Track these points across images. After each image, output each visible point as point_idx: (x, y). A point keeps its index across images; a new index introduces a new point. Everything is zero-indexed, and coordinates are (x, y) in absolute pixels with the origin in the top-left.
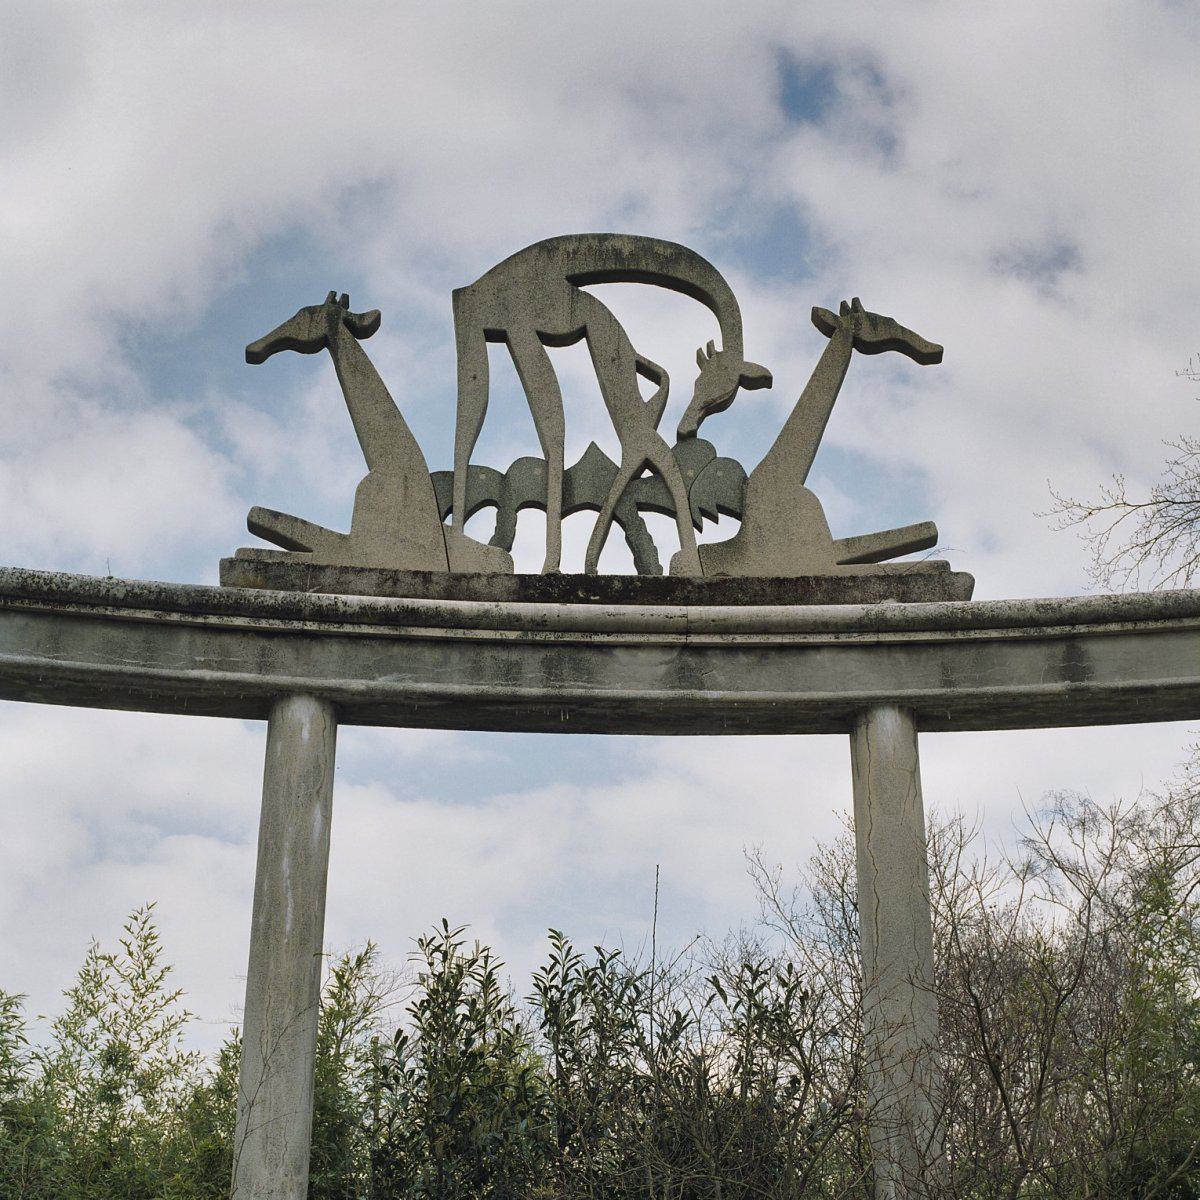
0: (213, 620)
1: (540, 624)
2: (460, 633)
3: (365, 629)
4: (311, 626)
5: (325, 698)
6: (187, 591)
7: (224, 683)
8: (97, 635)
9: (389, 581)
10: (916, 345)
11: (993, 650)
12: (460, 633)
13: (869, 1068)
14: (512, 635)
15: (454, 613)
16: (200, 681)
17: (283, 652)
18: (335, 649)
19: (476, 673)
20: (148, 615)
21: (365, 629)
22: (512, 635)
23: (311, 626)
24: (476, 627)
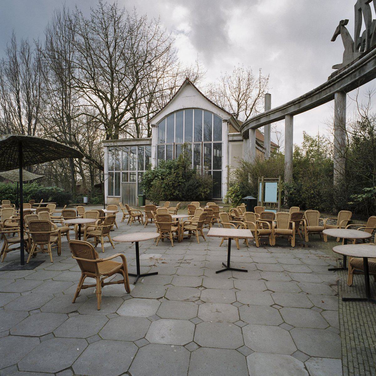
0: (324, 88)
1: (355, 67)
2: (348, 74)
3: (338, 80)
4: (333, 83)
5: (58, 157)
6: (319, 87)
7: (326, 96)
8: (315, 97)
9: (349, 65)
10: (357, 20)
11: (287, 109)
12: (348, 74)
13: (161, 50)
14: (353, 70)
15: (345, 72)
16: (324, 97)
17: (332, 88)
18: (337, 84)
19: (351, 79)
20: (318, 92)
21: (338, 80)
22: (353, 70)
23: (333, 83)
24: (349, 72)
